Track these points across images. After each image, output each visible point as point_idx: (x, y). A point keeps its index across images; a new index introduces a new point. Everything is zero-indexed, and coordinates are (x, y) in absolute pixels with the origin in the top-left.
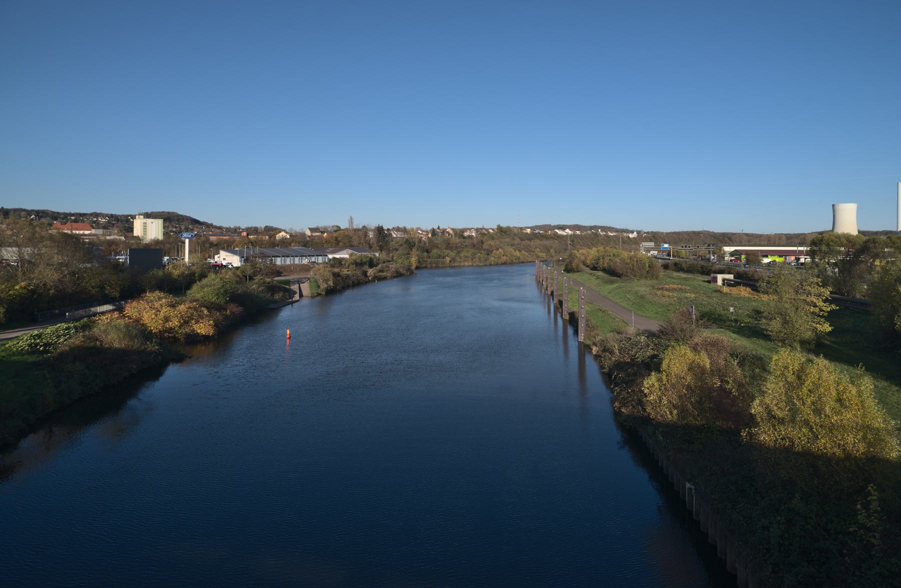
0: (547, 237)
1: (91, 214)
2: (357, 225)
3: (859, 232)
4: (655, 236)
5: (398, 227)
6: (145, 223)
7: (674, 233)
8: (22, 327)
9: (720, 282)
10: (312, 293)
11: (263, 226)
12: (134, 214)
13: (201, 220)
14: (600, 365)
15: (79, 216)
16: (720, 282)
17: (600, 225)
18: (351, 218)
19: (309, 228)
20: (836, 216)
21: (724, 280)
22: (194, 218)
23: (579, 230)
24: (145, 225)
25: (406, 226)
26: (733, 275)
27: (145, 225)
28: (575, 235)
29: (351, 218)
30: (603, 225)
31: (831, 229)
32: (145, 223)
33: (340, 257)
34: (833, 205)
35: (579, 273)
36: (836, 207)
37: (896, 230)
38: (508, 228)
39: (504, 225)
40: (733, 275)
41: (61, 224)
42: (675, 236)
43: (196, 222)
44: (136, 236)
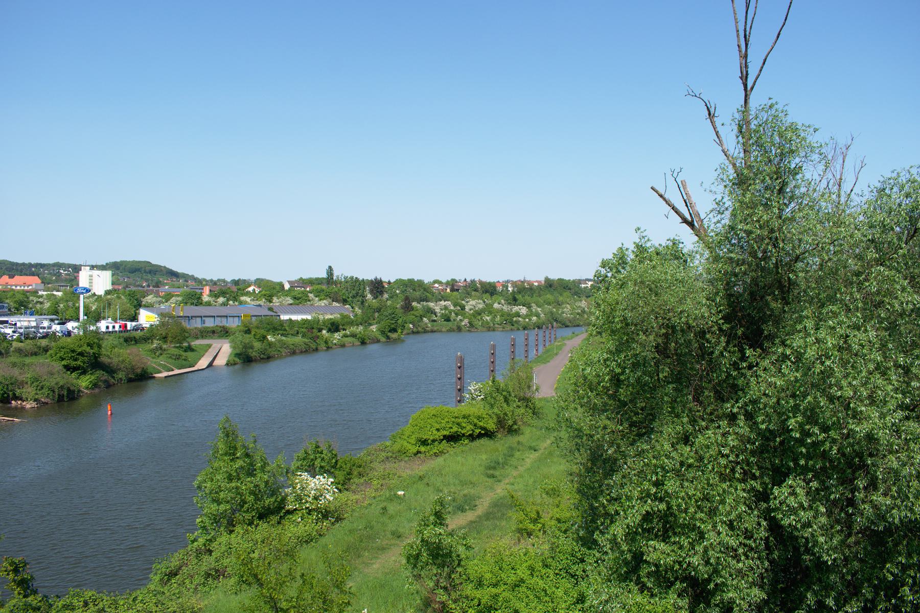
1: (55, 265)
2: (338, 277)
5: (547, 279)
6: (91, 276)
10: (228, 361)
11: (557, 278)
12: (78, 263)
13: (179, 271)
15: (39, 267)
17: (27, 262)
18: (330, 267)
19: (288, 281)
22: (170, 268)
24: (91, 278)
27: (91, 278)
29: (330, 267)
32: (91, 276)
33: (303, 320)
35: (473, 511)
39: (554, 276)
41: (9, 278)
43: (173, 274)
44: (395, 282)
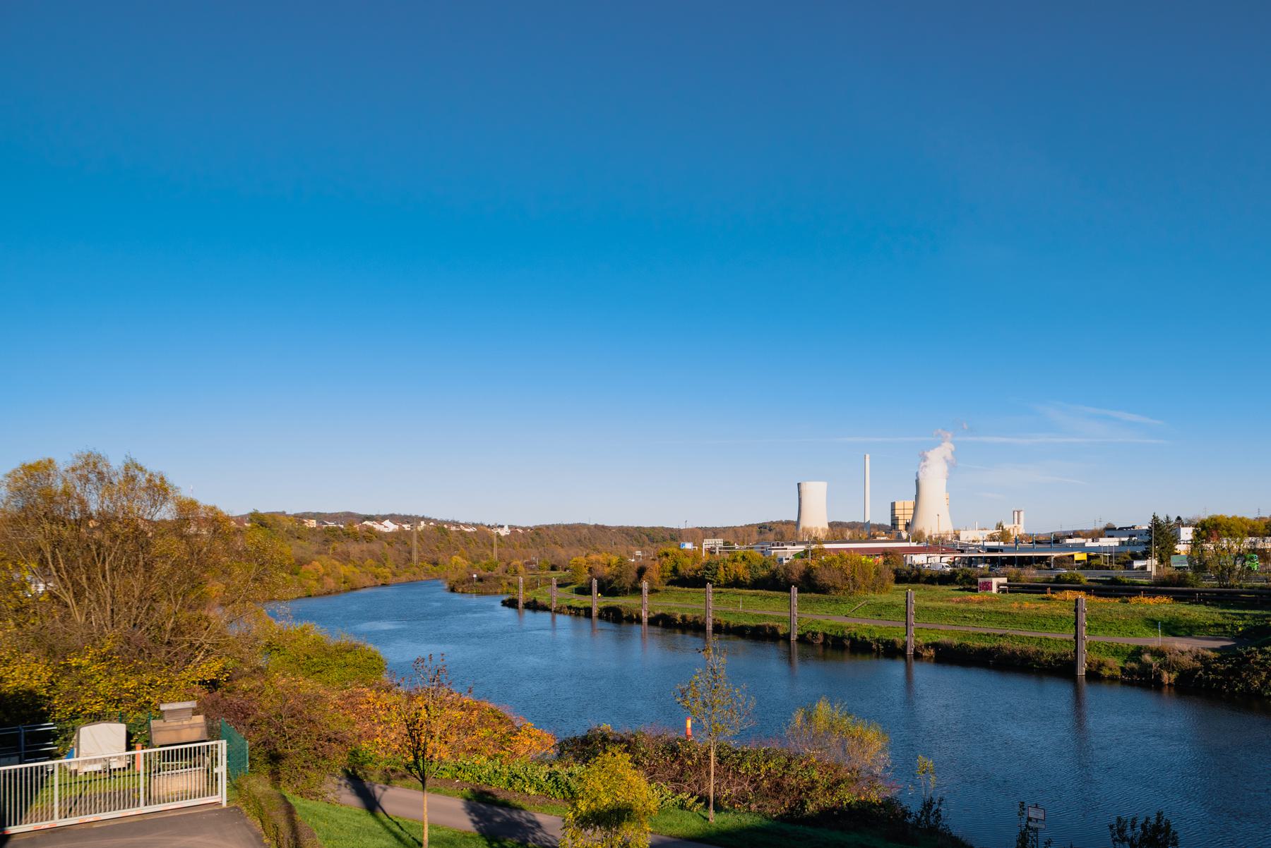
0: (356, 537)
3: (830, 525)
4: (540, 532)
7: (567, 527)
8: (111, 823)
9: (995, 590)
14: (296, 833)
16: (995, 590)
20: (802, 499)
21: (999, 585)
23: (408, 523)
25: (216, 505)
26: (1006, 579)
28: (402, 531)
30: (409, 514)
31: (795, 519)
34: (799, 484)
36: (803, 488)
37: (863, 522)
38: (273, 515)
40: (1006, 579)
42: (568, 532)
